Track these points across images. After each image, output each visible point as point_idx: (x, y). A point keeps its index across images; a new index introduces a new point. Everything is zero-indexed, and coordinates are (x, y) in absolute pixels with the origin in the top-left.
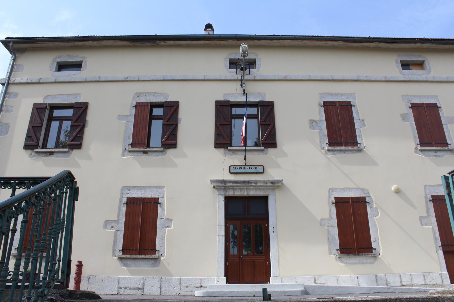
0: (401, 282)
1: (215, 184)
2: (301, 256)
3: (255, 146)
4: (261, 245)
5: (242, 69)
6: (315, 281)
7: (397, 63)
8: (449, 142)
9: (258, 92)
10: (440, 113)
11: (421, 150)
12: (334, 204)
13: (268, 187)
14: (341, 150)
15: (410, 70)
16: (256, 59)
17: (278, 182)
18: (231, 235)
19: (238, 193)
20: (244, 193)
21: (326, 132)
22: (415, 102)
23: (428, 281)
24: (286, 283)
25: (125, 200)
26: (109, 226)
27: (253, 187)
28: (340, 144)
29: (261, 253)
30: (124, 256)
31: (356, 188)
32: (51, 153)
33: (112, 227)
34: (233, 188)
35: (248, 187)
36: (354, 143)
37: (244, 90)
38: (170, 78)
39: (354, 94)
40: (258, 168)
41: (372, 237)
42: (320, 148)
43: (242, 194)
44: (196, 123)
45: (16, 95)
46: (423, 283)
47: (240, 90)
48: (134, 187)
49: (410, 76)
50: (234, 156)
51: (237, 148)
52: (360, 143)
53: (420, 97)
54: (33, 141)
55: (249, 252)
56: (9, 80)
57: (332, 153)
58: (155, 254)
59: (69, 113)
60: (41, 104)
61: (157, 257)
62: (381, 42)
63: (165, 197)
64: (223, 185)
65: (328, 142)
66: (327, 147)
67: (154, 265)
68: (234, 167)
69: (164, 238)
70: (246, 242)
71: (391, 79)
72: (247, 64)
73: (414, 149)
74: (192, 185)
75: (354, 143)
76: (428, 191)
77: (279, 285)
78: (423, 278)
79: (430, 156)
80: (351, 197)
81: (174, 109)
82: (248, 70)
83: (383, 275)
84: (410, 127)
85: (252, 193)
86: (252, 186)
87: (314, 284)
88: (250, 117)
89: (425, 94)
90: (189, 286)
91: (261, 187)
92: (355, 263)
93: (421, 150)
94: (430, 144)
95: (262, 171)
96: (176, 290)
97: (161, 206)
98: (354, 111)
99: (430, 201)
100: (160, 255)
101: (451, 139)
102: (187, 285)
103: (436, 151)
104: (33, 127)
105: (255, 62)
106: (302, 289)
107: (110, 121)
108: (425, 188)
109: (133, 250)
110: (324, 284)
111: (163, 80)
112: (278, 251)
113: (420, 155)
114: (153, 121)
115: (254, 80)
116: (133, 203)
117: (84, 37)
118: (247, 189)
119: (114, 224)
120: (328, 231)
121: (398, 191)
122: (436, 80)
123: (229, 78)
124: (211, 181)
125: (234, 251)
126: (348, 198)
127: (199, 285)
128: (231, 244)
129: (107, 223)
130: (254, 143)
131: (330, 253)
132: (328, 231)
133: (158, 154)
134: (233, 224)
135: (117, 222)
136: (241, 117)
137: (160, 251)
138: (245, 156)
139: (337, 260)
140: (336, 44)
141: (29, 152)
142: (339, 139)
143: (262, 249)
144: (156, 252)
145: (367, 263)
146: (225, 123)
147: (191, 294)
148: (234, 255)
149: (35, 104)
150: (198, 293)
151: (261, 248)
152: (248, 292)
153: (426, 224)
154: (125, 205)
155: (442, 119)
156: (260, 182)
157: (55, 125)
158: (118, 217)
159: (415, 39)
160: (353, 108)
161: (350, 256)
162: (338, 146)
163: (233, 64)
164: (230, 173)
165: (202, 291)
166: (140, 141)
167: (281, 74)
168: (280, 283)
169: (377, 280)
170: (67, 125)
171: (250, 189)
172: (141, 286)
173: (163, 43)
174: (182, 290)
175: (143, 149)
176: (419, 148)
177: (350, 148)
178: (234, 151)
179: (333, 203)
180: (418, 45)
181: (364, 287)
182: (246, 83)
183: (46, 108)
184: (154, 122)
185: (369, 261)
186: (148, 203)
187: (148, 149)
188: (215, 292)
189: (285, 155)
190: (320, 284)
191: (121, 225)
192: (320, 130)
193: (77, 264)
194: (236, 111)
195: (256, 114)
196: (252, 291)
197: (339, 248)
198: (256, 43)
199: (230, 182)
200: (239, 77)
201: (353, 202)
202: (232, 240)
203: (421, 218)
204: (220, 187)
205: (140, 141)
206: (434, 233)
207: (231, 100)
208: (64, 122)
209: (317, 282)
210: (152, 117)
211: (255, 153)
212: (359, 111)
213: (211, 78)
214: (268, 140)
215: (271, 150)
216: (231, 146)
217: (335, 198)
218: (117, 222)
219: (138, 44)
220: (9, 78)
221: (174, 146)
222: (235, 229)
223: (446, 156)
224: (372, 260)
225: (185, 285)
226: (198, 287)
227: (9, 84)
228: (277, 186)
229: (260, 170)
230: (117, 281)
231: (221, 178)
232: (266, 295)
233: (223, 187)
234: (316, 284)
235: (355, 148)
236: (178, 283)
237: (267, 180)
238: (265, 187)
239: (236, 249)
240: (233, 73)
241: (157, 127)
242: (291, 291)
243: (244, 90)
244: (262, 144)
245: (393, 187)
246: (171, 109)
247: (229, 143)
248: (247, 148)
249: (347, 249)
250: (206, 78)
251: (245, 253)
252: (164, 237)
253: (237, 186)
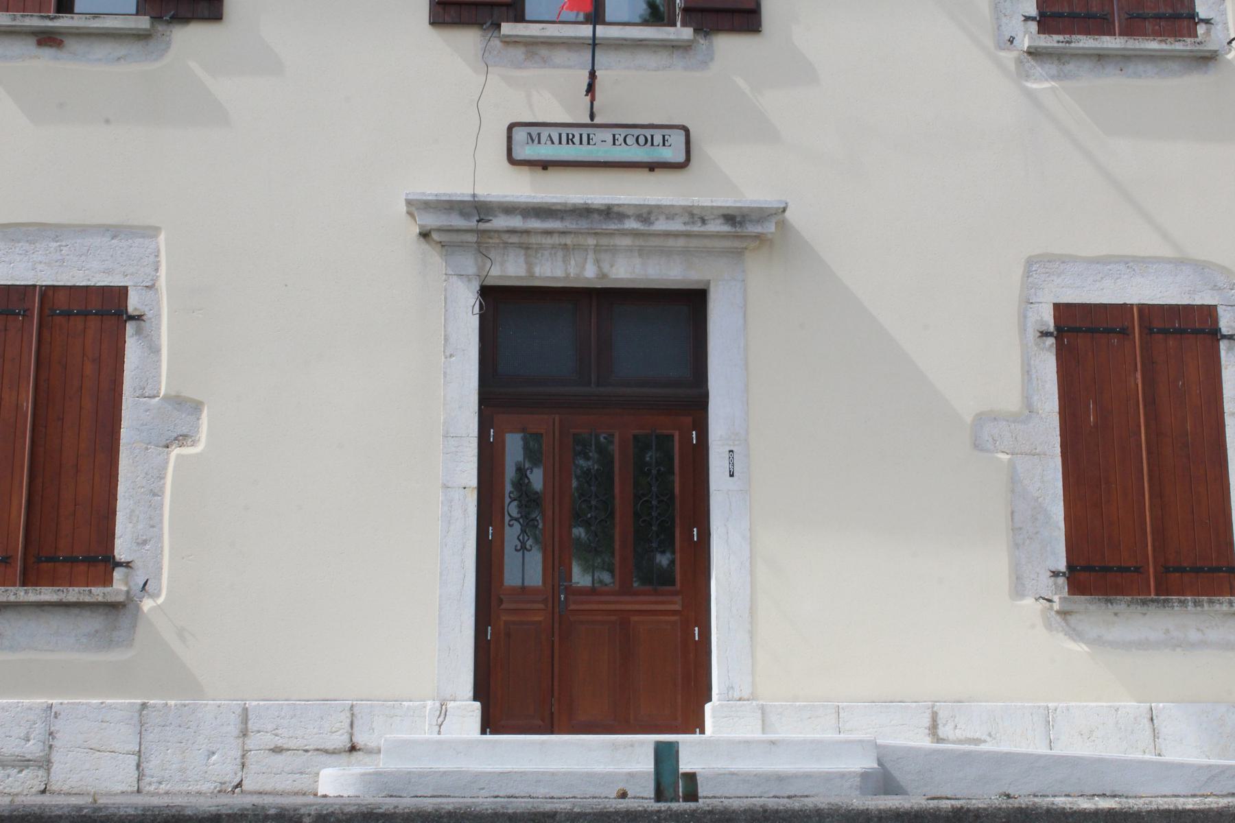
1: (431, 220)
3: (645, 23)
4: (667, 544)
6: (934, 728)
12: (1051, 341)
13: (708, 243)
14: (1101, 57)
18: (508, 488)
19: (551, 270)
24: (786, 730)
27: (626, 241)
28: (1098, 24)
29: (664, 579)
31: (1169, 261)
34: (523, 242)
35: (604, 241)
36: (1176, 17)
40: (658, 139)
43: (573, 271)
50: (532, 73)
52: (1207, 21)
55: (606, 577)
57: (1052, 68)
58: (107, 581)
61: (121, 598)
63: (162, 283)
64: (472, 224)
65: (1033, 12)
66: (1028, 37)
67: (107, 642)
68: (534, 131)
70: (587, 524)
77: (747, 743)
80: (1143, 308)
85: (627, 270)
87: (926, 743)
90: (292, 744)
91: (671, 242)
92: (1144, 645)
95: (681, 158)
96: (223, 768)
97: (139, 332)
100: (136, 588)
102: (280, 742)
110: (977, 741)
112: (752, 573)
118: (597, 249)
124: (409, 203)
125: (525, 569)
126: (1124, 309)
127: (341, 740)
128: (512, 533)
131: (1018, 589)
132: (1014, 480)
133: (121, 49)
137: (138, 564)
138: (593, 75)
139: (1049, 626)
143: (673, 562)
144: (118, 574)
145: (1203, 644)
147: (298, 786)
150: (335, 783)
151: (663, 560)
161: (1121, 605)
162: (1088, 32)
164: (512, 161)
165: (357, 770)
168: (758, 735)
171: (613, 250)
172: (33, 749)
174: (252, 767)
175: (34, 22)
177: (1153, 45)
179: (1045, 334)
181: (1182, 766)
186: (68, 314)
187: (64, 22)
188: (422, 775)
190: (960, 742)
196: (611, 768)
197: (1062, 565)
199: (509, 209)
201: (1148, 330)
202: (513, 509)
209: (942, 732)
215: (728, 46)
216: (520, 18)
217: (1057, 307)
222: (533, 455)
225: (270, 740)
226: (334, 752)
231: (461, 189)
232: (670, 778)
233: (472, 238)
234: (940, 740)
235: (1178, 46)
236: (233, 729)
237: (705, 201)
238: (694, 243)
239: (535, 559)
242: (808, 776)
244: (686, 10)
248: (602, 31)
249: (1106, 569)
251: (580, 578)
252: (157, 493)
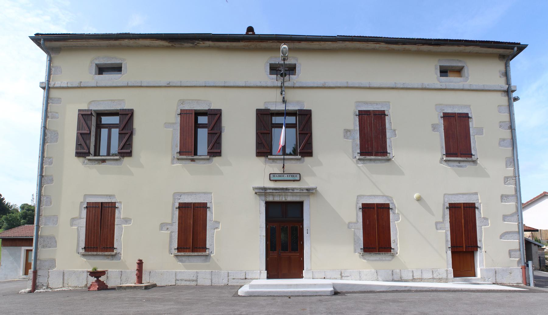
0: (413, 276)
1: (257, 191)
2: (332, 259)
5: (282, 75)
6: (341, 274)
7: (436, 69)
8: (473, 153)
9: (298, 100)
10: (470, 123)
11: (446, 161)
14: (371, 160)
15: (447, 76)
16: (295, 64)
17: (313, 189)
19: (277, 199)
20: (283, 199)
21: (358, 142)
22: (447, 112)
23: (435, 276)
25: (177, 205)
26: (165, 228)
28: (370, 154)
30: (179, 254)
32: (104, 161)
33: (168, 229)
34: (272, 194)
36: (384, 152)
37: (284, 98)
38: (212, 85)
39: (389, 102)
41: (392, 239)
42: (351, 157)
44: (239, 132)
45: (59, 100)
46: (431, 277)
47: (280, 99)
48: (184, 193)
49: (447, 84)
50: (273, 164)
51: (277, 157)
53: (453, 106)
54: (83, 149)
56: (49, 84)
58: (206, 251)
59: (115, 120)
60: (85, 110)
62: (424, 44)
69: (213, 238)
71: (427, 87)
72: (287, 69)
73: (439, 159)
74: (236, 189)
75: (384, 152)
76: (446, 199)
78: (431, 273)
79: (453, 166)
81: (217, 117)
82: (287, 76)
83: (398, 271)
84: (438, 139)
85: (290, 199)
88: (288, 126)
89: (456, 103)
92: (376, 260)
93: (446, 161)
94: (456, 155)
98: (387, 121)
99: (447, 208)
101: (476, 150)
103: (459, 161)
104: (81, 134)
105: (295, 68)
107: (157, 130)
108: (444, 197)
109: (187, 248)
111: (205, 86)
113: (444, 166)
114: (199, 129)
115: (294, 87)
116: (185, 207)
117: (118, 34)
118: (285, 195)
119: (169, 227)
120: (355, 233)
121: (419, 199)
122: (472, 88)
123: (269, 84)
126: (374, 204)
127: (244, 277)
129: (163, 226)
131: (355, 252)
132: (355, 233)
133: (205, 162)
135: (171, 224)
136: (280, 126)
140: (377, 46)
141: (82, 159)
142: (370, 149)
145: (386, 260)
146: (265, 132)
149: (79, 110)
153: (441, 229)
154: (178, 210)
155: (471, 129)
156: (297, 189)
157: (104, 132)
158: (172, 220)
159: (461, 40)
160: (386, 117)
163: (274, 69)
166: (188, 150)
167: (319, 82)
169: (393, 275)
170: (115, 132)
171: (288, 195)
172: (194, 278)
173: (202, 44)
174: (230, 282)
176: (445, 159)
177: (380, 158)
180: (462, 48)
182: (286, 90)
183: (91, 114)
184: (199, 130)
185: (387, 259)
186: (197, 207)
187: (195, 157)
189: (320, 164)
191: (176, 227)
192: (354, 139)
193: (138, 262)
194: (276, 120)
195: (294, 122)
198: (297, 45)
199: (270, 189)
200: (279, 85)
201: (377, 207)
203: (437, 223)
205: (188, 150)
206: (446, 236)
207: (271, 109)
208: (112, 129)
210: (197, 126)
211: (293, 162)
212: (392, 121)
213: (252, 85)
214: (304, 148)
215: (307, 159)
216: (271, 155)
218: (171, 224)
219: (177, 45)
220: (49, 81)
221: (218, 154)
223: (468, 166)
224: (389, 258)
227: (49, 88)
229: (296, 177)
230: (174, 274)
231: (261, 185)
236: (226, 275)
240: (273, 80)
241: (203, 134)
243: (284, 98)
244: (300, 153)
245: (416, 196)
246: (215, 116)
248: (285, 157)
250: (248, 85)
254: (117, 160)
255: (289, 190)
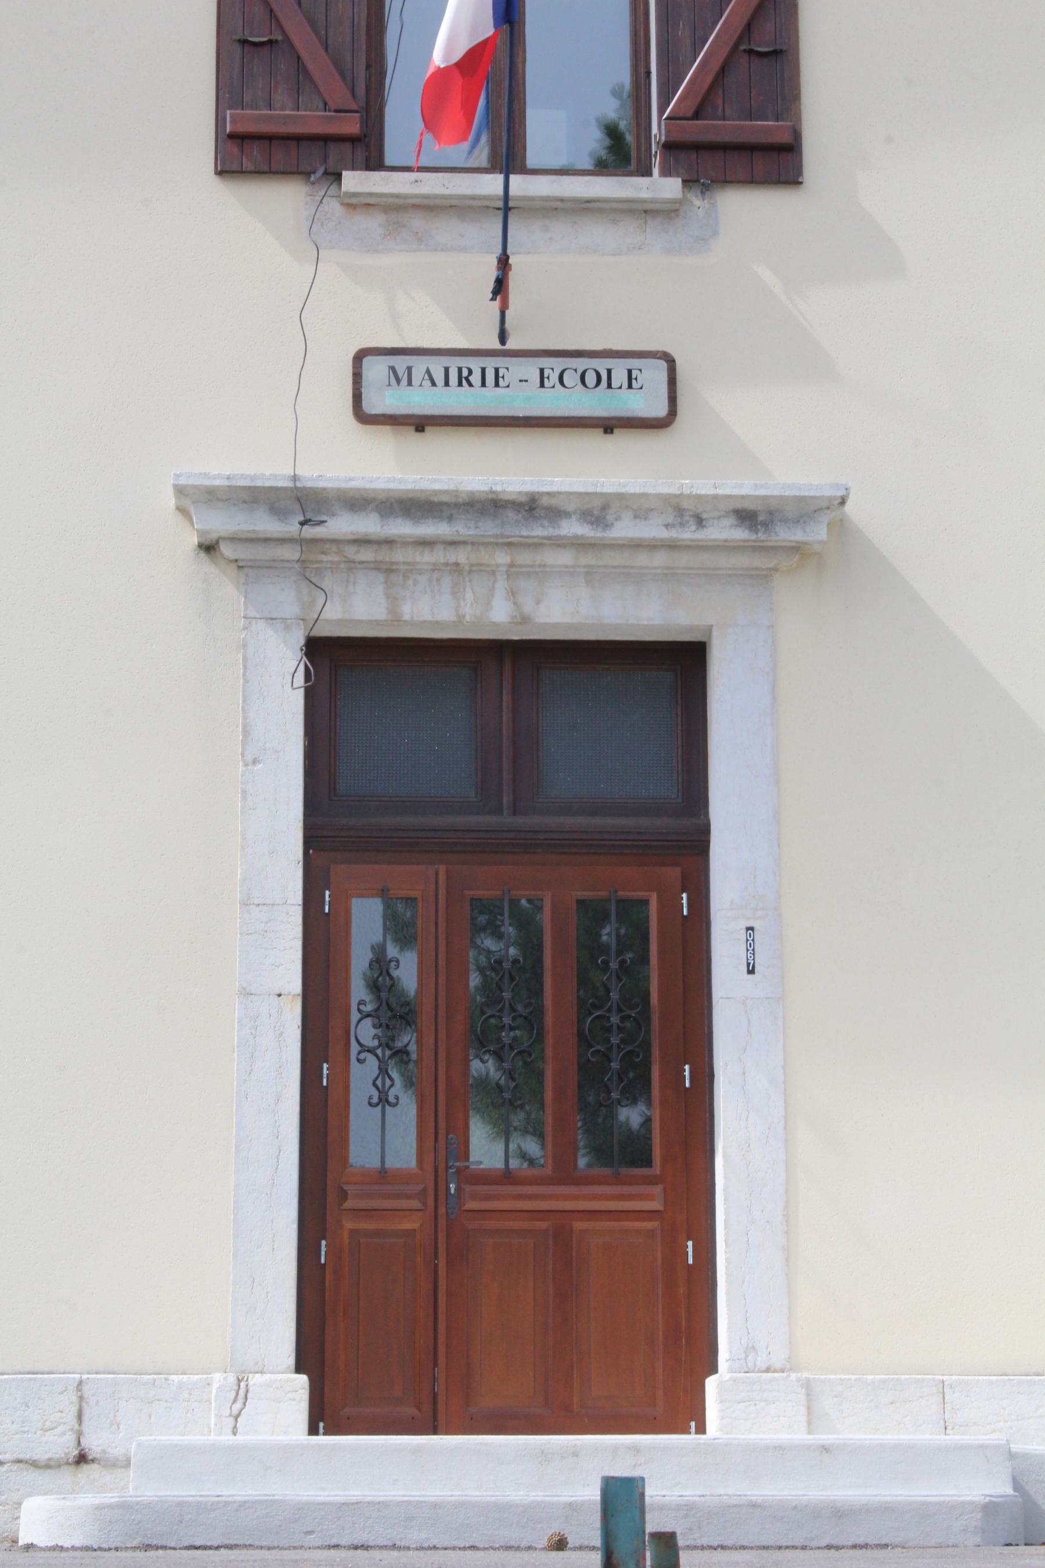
1: (220, 522)
3: (601, 168)
4: (637, 1088)
17: (806, 510)
19: (431, 611)
20: (490, 611)
27: (565, 558)
29: (630, 1154)
34: (381, 559)
35: (524, 558)
40: (619, 377)
50: (396, 260)
51: (433, 185)
55: (532, 1146)
64: (291, 528)
68: (401, 363)
77: (781, 1449)
85: (563, 610)
86: (559, 543)
91: (642, 559)
95: (660, 410)
106: (997, 1486)
118: (513, 571)
121: (751, 971)
124: (180, 491)
125: (386, 1136)
127: (62, 1445)
130: (594, 141)
134: (383, 893)
138: (504, 263)
148: (383, 1175)
151: (631, 1116)
152: (501, 1510)
156: (639, 507)
164: (362, 416)
165: (88, 1500)
168: (800, 1436)
171: (541, 574)
178: (396, 208)
188: (201, 1507)
196: (537, 1496)
199: (357, 502)
202: (366, 1032)
204: (261, 553)
215: (745, 211)
216: (375, 162)
222: (400, 929)
226: (47, 1465)
228: (797, 549)
229: (634, 394)
231: (272, 468)
233: (291, 553)
237: (704, 487)
238: (683, 559)
239: (405, 1114)
242: (888, 1509)
244: (669, 147)
247: (351, 126)
251: (485, 1149)
253: (426, 543)
254: (647, 212)
255: (555, 514)
